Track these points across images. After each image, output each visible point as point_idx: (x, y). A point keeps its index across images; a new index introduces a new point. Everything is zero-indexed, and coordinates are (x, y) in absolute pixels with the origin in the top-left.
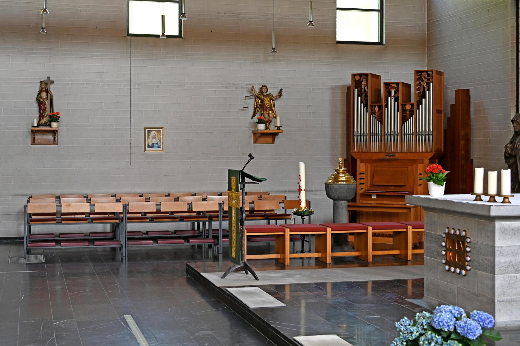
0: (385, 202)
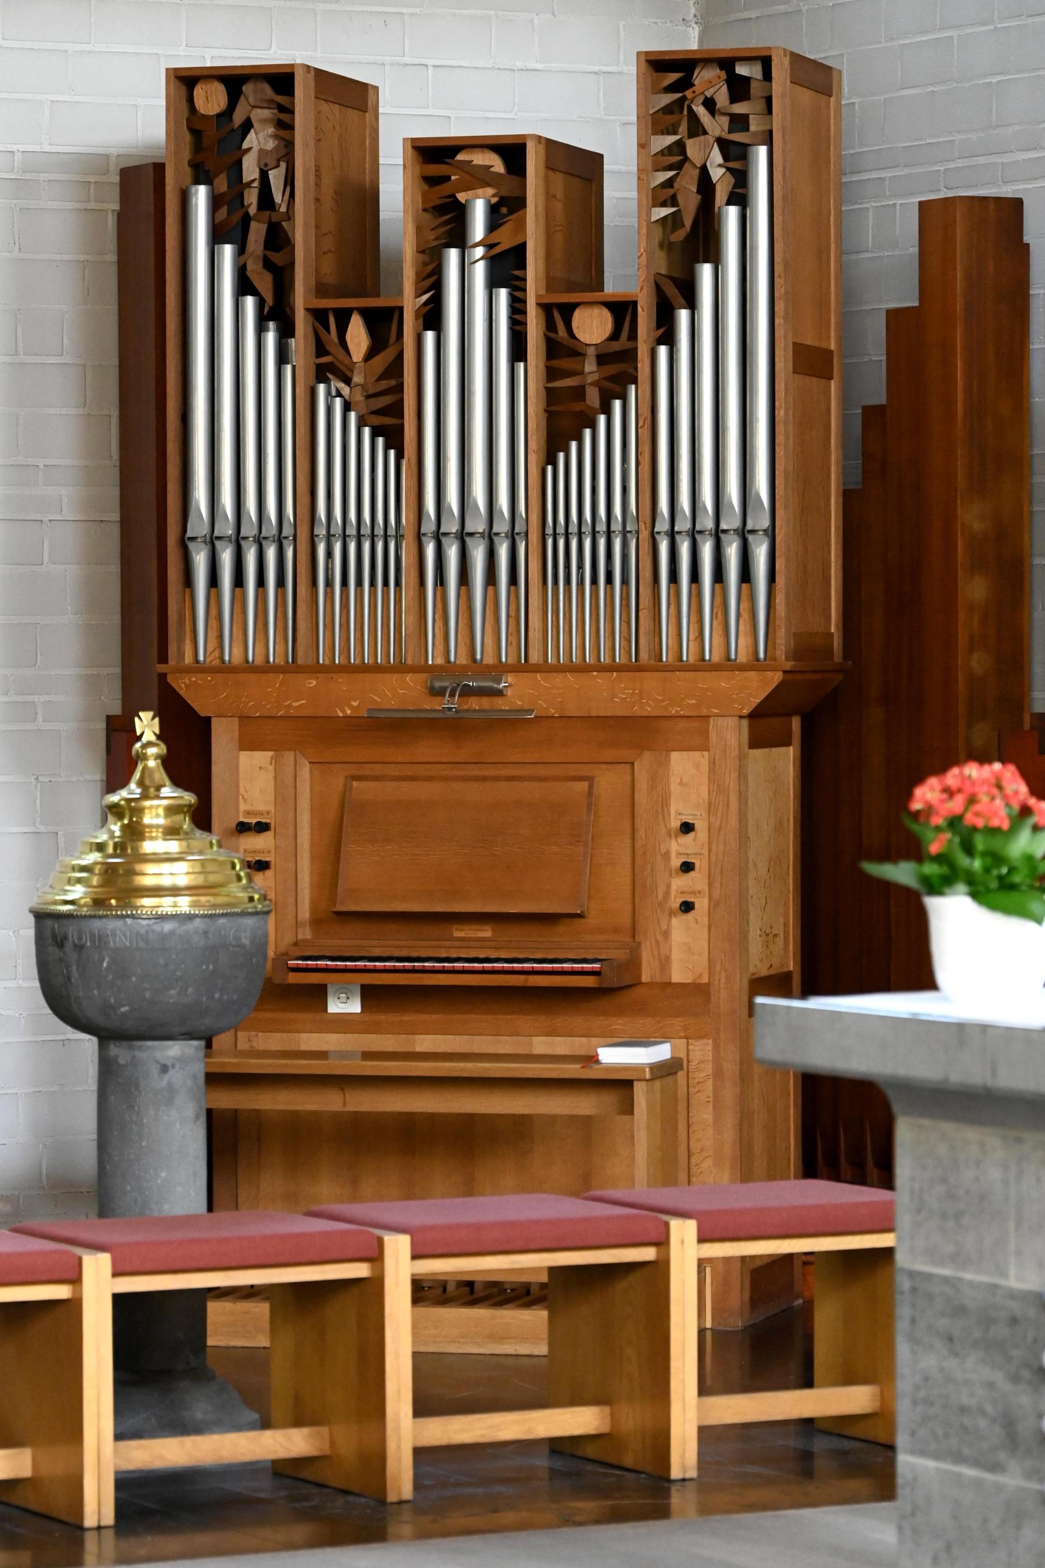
0: (424, 1043)
